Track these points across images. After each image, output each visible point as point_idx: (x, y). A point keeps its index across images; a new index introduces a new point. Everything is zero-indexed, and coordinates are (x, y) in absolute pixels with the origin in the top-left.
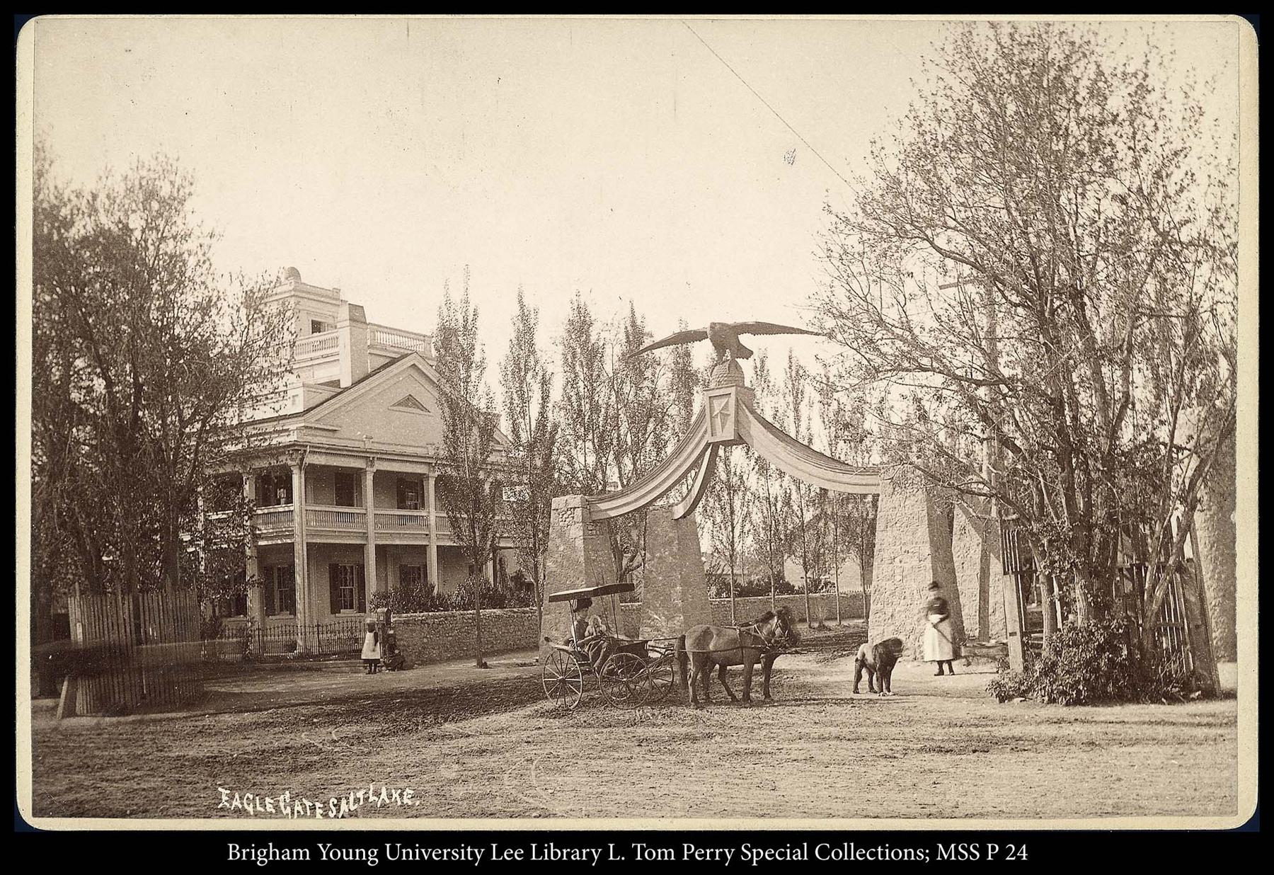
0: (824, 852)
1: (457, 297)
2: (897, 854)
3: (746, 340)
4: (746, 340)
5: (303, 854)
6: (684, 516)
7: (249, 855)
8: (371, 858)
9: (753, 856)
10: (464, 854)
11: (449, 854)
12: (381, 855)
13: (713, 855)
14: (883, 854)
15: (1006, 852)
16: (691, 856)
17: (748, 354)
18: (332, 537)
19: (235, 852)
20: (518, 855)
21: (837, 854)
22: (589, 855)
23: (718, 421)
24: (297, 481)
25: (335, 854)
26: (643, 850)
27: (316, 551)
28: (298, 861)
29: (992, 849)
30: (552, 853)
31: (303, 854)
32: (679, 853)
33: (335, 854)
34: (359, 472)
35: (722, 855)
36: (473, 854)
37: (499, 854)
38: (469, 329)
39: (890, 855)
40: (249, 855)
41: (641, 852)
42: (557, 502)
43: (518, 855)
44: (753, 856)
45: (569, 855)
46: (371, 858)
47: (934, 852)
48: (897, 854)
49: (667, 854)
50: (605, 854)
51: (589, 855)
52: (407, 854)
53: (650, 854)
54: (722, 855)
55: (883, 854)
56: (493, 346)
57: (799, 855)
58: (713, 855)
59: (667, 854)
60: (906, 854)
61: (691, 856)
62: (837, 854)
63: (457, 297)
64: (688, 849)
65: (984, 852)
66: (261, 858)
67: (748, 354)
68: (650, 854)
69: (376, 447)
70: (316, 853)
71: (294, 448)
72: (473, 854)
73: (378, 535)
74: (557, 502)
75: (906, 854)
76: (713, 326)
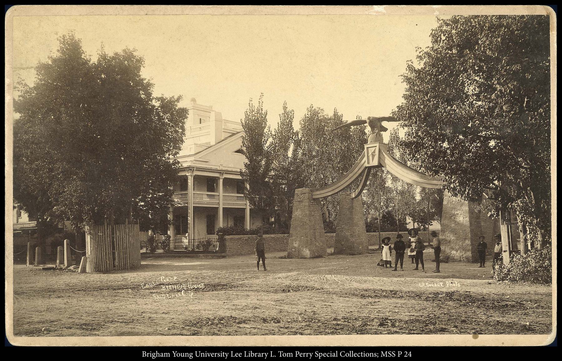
0: (343, 354)
1: (256, 105)
2: (367, 355)
3: (385, 124)
4: (385, 124)
5: (168, 355)
6: (356, 197)
7: (149, 355)
8: (191, 356)
9: (319, 355)
10: (222, 355)
11: (217, 355)
12: (194, 355)
13: (305, 355)
14: (363, 355)
15: (404, 354)
16: (298, 355)
17: (385, 130)
18: (234, 205)
19: (144, 354)
20: (240, 355)
21: (347, 355)
22: (264, 355)
23: (371, 158)
24: (190, 182)
25: (178, 355)
26: (282, 353)
27: (198, 210)
28: (166, 357)
29: (400, 353)
30: (251, 354)
31: (168, 355)
32: (294, 354)
33: (178, 355)
34: (219, 178)
35: (309, 355)
36: (225, 355)
37: (234, 355)
38: (264, 120)
39: (365, 355)
40: (149, 355)
41: (281, 354)
42: (298, 191)
43: (240, 355)
44: (319, 355)
45: (257, 355)
46: (191, 356)
47: (380, 354)
48: (367, 355)
49: (290, 355)
50: (269, 355)
51: (264, 355)
52: (203, 355)
53: (284, 355)
54: (309, 355)
55: (363, 355)
56: (273, 124)
57: (334, 355)
58: (305, 355)
59: (290, 355)
60: (370, 355)
61: (298, 355)
62: (347, 355)
63: (256, 105)
64: (297, 353)
65: (397, 354)
66: (153, 356)
67: (385, 130)
68: (284, 355)
69: (224, 169)
70: (172, 355)
71: (189, 169)
72: (225, 355)
73: (224, 204)
74: (298, 191)
75: (370, 355)
76: (369, 118)
